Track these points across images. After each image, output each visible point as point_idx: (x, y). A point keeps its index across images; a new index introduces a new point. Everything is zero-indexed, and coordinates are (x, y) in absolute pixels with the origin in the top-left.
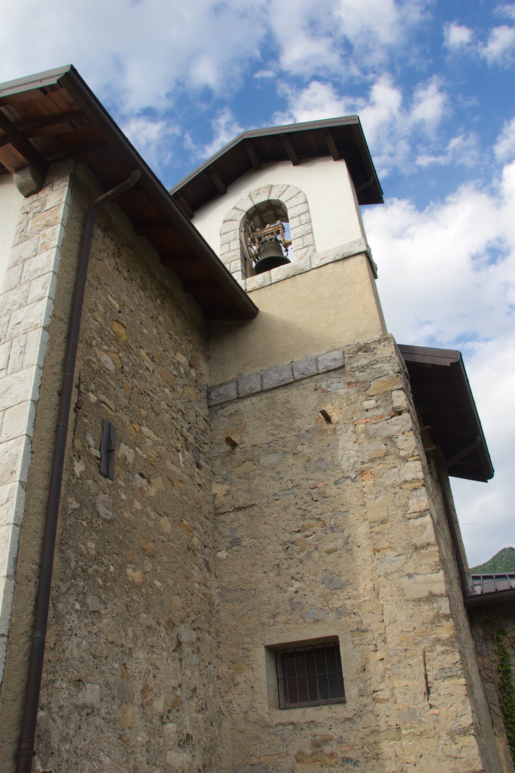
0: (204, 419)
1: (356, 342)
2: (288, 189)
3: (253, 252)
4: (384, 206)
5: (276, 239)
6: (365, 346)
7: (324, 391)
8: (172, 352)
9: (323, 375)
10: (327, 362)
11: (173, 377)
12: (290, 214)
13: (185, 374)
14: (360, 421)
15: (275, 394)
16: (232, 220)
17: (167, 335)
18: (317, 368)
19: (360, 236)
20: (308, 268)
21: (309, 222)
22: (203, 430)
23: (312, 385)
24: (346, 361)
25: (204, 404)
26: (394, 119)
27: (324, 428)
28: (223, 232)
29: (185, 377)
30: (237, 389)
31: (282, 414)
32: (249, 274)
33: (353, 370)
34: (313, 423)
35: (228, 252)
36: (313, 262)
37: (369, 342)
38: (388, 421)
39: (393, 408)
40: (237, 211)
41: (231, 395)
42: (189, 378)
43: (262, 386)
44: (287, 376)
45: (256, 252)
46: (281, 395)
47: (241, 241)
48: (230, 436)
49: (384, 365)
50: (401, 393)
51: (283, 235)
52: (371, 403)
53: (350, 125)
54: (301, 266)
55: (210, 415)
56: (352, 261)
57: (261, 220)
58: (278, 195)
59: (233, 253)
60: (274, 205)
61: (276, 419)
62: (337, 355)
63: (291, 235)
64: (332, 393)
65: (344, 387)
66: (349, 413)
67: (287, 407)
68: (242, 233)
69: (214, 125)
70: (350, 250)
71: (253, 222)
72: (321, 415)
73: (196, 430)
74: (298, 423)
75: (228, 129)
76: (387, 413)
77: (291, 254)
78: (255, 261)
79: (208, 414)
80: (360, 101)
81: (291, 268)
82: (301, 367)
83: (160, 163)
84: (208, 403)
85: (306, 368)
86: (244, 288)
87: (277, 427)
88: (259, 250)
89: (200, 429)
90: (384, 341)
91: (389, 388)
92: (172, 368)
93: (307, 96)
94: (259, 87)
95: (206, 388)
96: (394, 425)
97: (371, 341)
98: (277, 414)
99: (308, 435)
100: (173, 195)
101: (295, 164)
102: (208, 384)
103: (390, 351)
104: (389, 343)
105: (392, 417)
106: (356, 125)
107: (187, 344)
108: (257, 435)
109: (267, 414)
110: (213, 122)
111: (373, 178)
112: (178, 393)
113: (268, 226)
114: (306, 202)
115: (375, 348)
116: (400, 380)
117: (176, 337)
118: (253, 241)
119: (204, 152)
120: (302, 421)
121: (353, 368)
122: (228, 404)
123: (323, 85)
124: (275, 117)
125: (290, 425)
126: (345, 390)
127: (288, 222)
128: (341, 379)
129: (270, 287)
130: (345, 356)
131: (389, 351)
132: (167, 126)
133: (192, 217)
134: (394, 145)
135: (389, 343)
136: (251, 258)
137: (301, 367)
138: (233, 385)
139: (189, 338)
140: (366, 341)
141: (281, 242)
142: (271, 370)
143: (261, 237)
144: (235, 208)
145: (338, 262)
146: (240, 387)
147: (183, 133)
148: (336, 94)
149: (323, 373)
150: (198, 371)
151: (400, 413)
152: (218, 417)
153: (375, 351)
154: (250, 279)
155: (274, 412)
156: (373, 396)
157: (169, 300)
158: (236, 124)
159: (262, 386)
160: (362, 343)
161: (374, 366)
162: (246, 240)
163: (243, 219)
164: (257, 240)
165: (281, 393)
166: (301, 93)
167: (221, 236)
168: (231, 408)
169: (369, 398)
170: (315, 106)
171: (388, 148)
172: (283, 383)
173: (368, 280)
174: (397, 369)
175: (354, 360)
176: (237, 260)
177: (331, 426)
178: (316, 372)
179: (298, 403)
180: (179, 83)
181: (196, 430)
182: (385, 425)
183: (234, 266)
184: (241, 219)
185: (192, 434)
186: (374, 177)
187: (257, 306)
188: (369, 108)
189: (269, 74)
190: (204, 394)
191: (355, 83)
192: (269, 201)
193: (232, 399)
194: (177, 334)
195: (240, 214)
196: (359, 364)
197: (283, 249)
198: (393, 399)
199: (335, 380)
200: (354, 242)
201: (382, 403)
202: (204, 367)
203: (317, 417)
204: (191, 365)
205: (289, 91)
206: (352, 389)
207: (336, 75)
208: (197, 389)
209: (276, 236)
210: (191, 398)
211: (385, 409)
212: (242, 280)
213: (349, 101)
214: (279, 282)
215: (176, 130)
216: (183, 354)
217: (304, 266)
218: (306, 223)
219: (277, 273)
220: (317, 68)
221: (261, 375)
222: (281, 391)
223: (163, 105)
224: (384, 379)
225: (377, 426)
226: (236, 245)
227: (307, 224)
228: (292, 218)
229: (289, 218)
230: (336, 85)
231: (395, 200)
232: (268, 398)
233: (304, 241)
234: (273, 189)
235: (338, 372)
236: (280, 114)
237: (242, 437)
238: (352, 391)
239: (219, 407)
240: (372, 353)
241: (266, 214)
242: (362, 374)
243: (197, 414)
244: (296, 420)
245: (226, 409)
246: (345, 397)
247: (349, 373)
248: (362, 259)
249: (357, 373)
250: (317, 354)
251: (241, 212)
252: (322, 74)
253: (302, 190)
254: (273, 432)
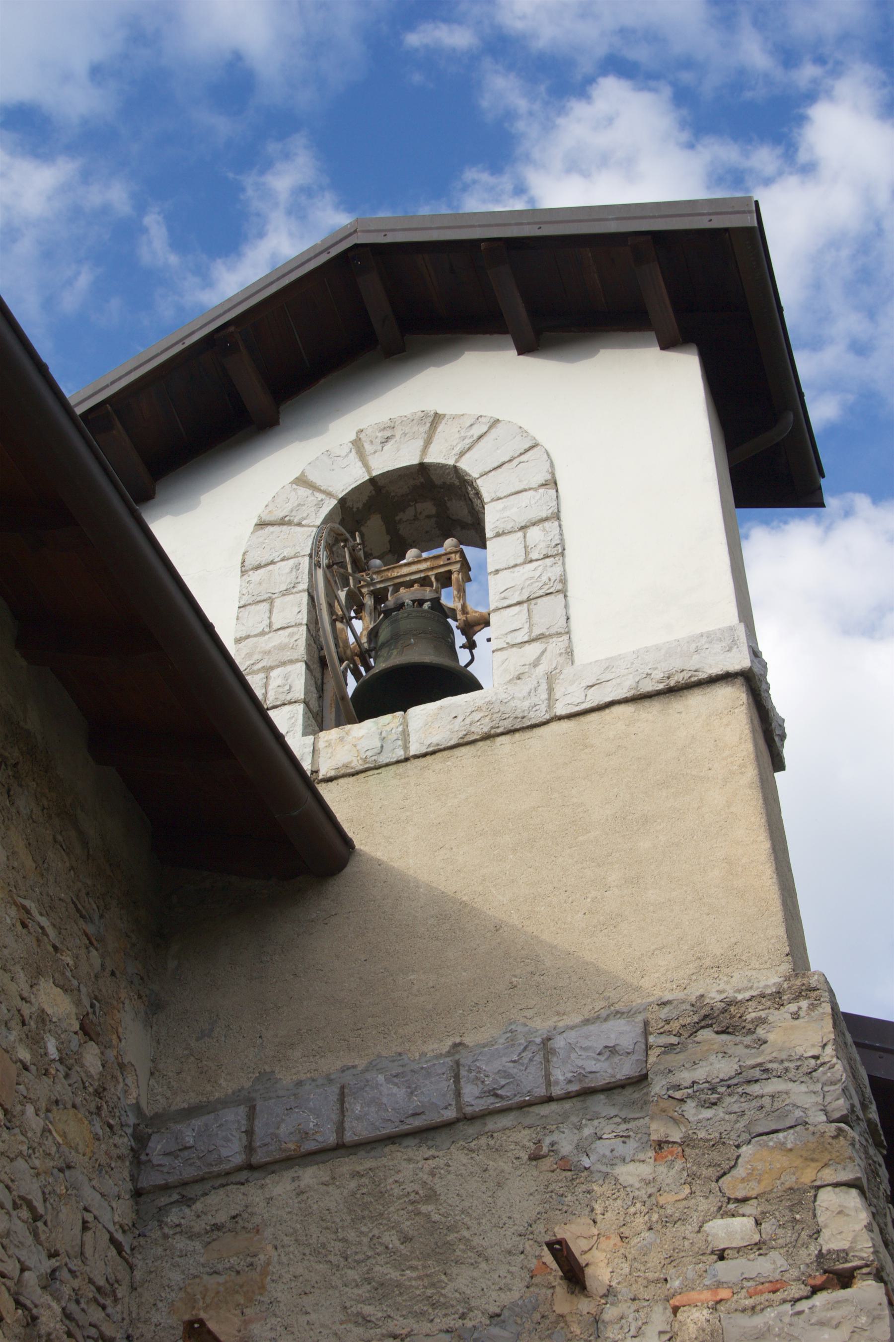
0: (113, 1240)
1: (694, 992)
2: (494, 433)
3: (352, 640)
4: (818, 522)
5: (436, 603)
6: (724, 1011)
7: (566, 1165)
8: (22, 977)
9: (567, 1105)
10: (585, 1055)
11: (14, 1069)
12: (493, 518)
13: (61, 1060)
14: (694, 1295)
15: (384, 1160)
16: (289, 523)
17: (13, 911)
18: (548, 1076)
19: (730, 614)
20: (542, 714)
21: (558, 552)
22: (101, 1282)
23: (525, 1136)
24: (652, 1059)
25: (118, 1181)
26: (878, 224)
27: (559, 1309)
28: (251, 562)
29: (61, 1075)
30: (250, 1132)
31: (406, 1239)
32: (330, 715)
33: (678, 1095)
34: (518, 1285)
35: (263, 633)
36: (559, 692)
37: (740, 997)
38: (799, 1306)
39: (820, 1255)
40: (310, 492)
41: (225, 1152)
42: (74, 1077)
43: (340, 1129)
44: (435, 1097)
45: (364, 640)
46: (407, 1167)
47: (311, 598)
48: (202, 1315)
49: (791, 1085)
50: (852, 1199)
51: (462, 591)
52: (735, 1229)
53: (726, 230)
54: (516, 703)
55: (137, 1228)
56: (696, 700)
57: (388, 532)
58: (457, 450)
59: (281, 637)
60: (438, 482)
61: (381, 1259)
62: (622, 1033)
63: (491, 592)
64: (596, 1176)
65: (641, 1156)
66: (655, 1259)
67: (428, 1216)
68: (320, 573)
69: (250, 192)
70: (694, 663)
71: (362, 536)
72: (548, 1258)
73: (76, 1283)
74: (463, 1281)
75: (298, 211)
76: (794, 1273)
77: (487, 660)
78: (357, 674)
79: (128, 1221)
80: (764, 158)
81: (479, 709)
82: (490, 1067)
83: (49, 303)
84: (133, 1179)
85: (506, 1075)
86: (307, 766)
87: (382, 1290)
88: (373, 634)
89: (91, 1281)
90: (796, 998)
91: (808, 1176)
92: (13, 1036)
93: (578, 125)
94: (417, 78)
95: (132, 1120)
96: (821, 1324)
97: (747, 995)
98: (386, 1239)
99: (495, 1331)
100: (80, 415)
101: (523, 350)
102: (144, 1105)
103: (817, 1039)
104: (812, 1007)
105: (815, 1290)
106: (749, 230)
107: (83, 952)
108: (303, 1319)
109: (352, 1235)
110: (249, 181)
111: (791, 416)
112: (24, 1134)
113: (411, 554)
114: (552, 483)
115: (762, 1021)
116: (849, 1151)
117: (44, 921)
118: (355, 602)
119: (208, 282)
120: (476, 1273)
121: (678, 1087)
122: (207, 1186)
123: (641, 89)
124: (465, 188)
125: (433, 1285)
126: (645, 1170)
127: (484, 547)
128: (629, 1126)
129: (401, 768)
130: (651, 1039)
131: (805, 1035)
132: (86, 176)
133: (144, 494)
134: (872, 314)
135: (812, 1007)
136: (341, 661)
137: (490, 1067)
138: (235, 1116)
139: (91, 929)
140: (730, 993)
141: (453, 613)
142: (380, 1071)
143: (386, 589)
144: (302, 481)
145: (646, 703)
146: (258, 1124)
147: (141, 208)
148: (683, 124)
149: (568, 1096)
150: (111, 1054)
151: (845, 1279)
152: (166, 1237)
153: (760, 1032)
154: (333, 734)
155: (376, 1232)
156: (745, 1200)
157: (33, 785)
158: (329, 197)
159: (340, 1129)
160: (714, 997)
161: (755, 1089)
162: (331, 596)
163: (325, 522)
164: (369, 601)
165: (409, 1160)
166: (562, 111)
167: (244, 572)
168: (219, 1205)
169: (732, 1206)
170: (604, 160)
171: (848, 323)
172: (417, 1123)
173: (751, 773)
174: (840, 1106)
175: (681, 1056)
176: (291, 662)
177: (585, 1306)
178: (541, 1092)
179: (466, 1204)
180: (140, 35)
181: (76, 1283)
182: (787, 1319)
183: (279, 682)
184: (318, 522)
185: (58, 1300)
186: (796, 416)
187: (350, 834)
188: (792, 181)
189: (457, 38)
190: (124, 1142)
191: (748, 95)
192: (422, 468)
193: (226, 1167)
194: (49, 909)
195: (319, 505)
196: (700, 1074)
197: (460, 639)
198: (821, 1219)
199: (607, 1130)
200: (709, 637)
201: (780, 1231)
202: (133, 1040)
203: (533, 1264)
204: (87, 1031)
205: (522, 104)
206: (671, 1166)
207: (687, 63)
208: (97, 1123)
209: (438, 591)
210: (74, 1157)
211: (789, 1255)
212: (305, 734)
213: (727, 152)
214: (433, 753)
215: (117, 195)
216: (62, 987)
217: (526, 704)
218: (546, 557)
219: (429, 721)
220: (624, 32)
221: (343, 1087)
222: (410, 1153)
223: (79, 102)
224: (789, 1138)
225: (758, 1321)
226: (294, 610)
227: (549, 561)
228: (498, 535)
229: (489, 534)
230: (683, 97)
231: (862, 502)
232: (356, 1175)
233: (536, 619)
234: (441, 428)
235: (621, 1097)
236: (485, 177)
237: (246, 1323)
238: (669, 1173)
239: (176, 1197)
240: (748, 1040)
241: (410, 513)
242: (708, 1113)
243: (89, 1217)
244: (455, 1270)
245: (198, 1206)
246: (642, 1194)
247: (663, 1104)
248: (734, 697)
249: (690, 1108)
250: (550, 1023)
251: (320, 496)
252: (640, 54)
253: (540, 439)
254: (367, 1310)
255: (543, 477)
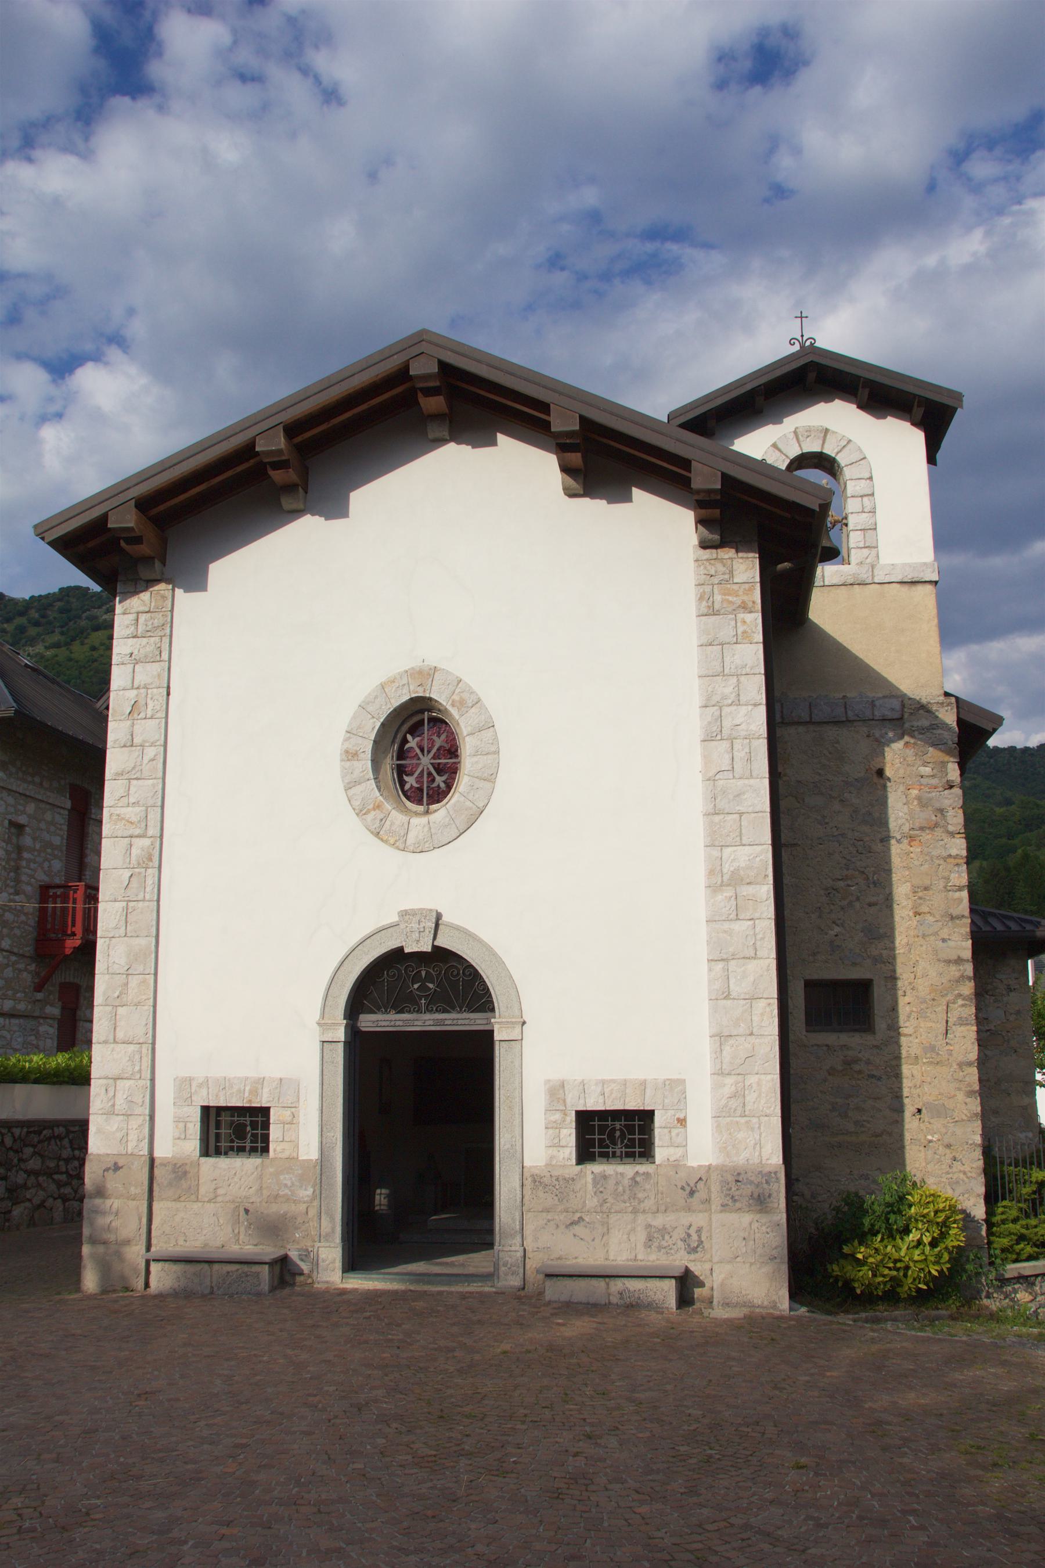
7: (877, 740)
23: (865, 729)
46: (831, 732)
52: (927, 770)
56: (920, 587)
62: (896, 704)
114: (871, 478)
151: (951, 787)
177: (882, 781)
196: (919, 723)
255: (867, 475)
